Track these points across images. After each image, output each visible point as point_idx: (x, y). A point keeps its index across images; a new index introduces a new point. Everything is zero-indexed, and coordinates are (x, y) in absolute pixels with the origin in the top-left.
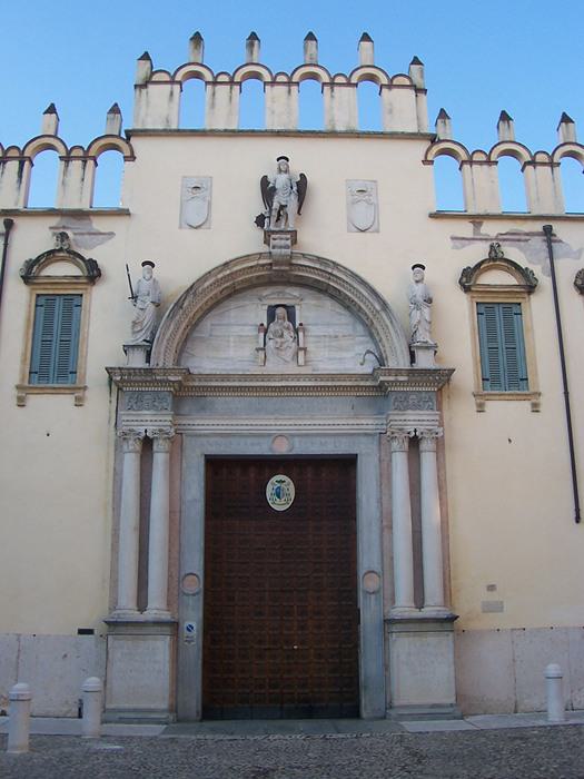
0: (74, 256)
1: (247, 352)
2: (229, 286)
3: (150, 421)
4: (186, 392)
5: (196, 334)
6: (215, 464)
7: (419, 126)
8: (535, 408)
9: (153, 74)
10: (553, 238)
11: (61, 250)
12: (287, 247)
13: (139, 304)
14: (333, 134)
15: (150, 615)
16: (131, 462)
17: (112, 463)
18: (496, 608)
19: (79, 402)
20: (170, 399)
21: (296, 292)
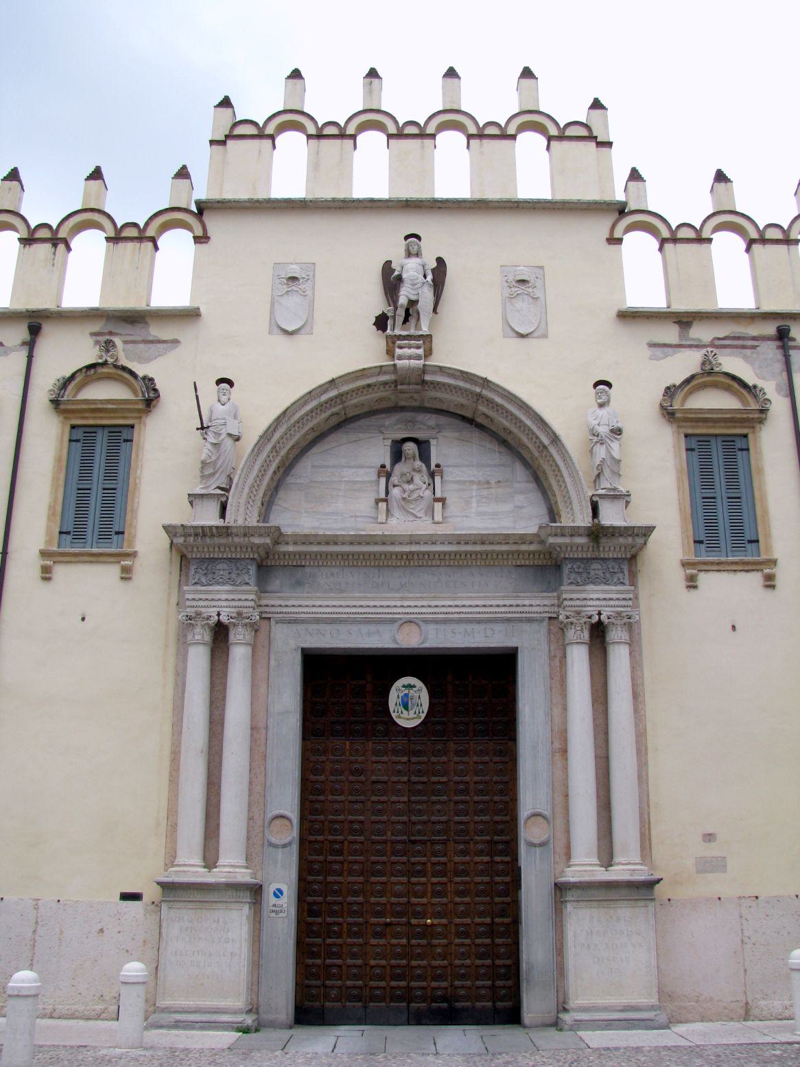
1: (364, 504)
2: (333, 417)
3: (224, 599)
5: (290, 480)
12: (418, 357)
16: (199, 658)
18: (715, 865)
19: (127, 574)
20: (253, 569)
21: (431, 420)
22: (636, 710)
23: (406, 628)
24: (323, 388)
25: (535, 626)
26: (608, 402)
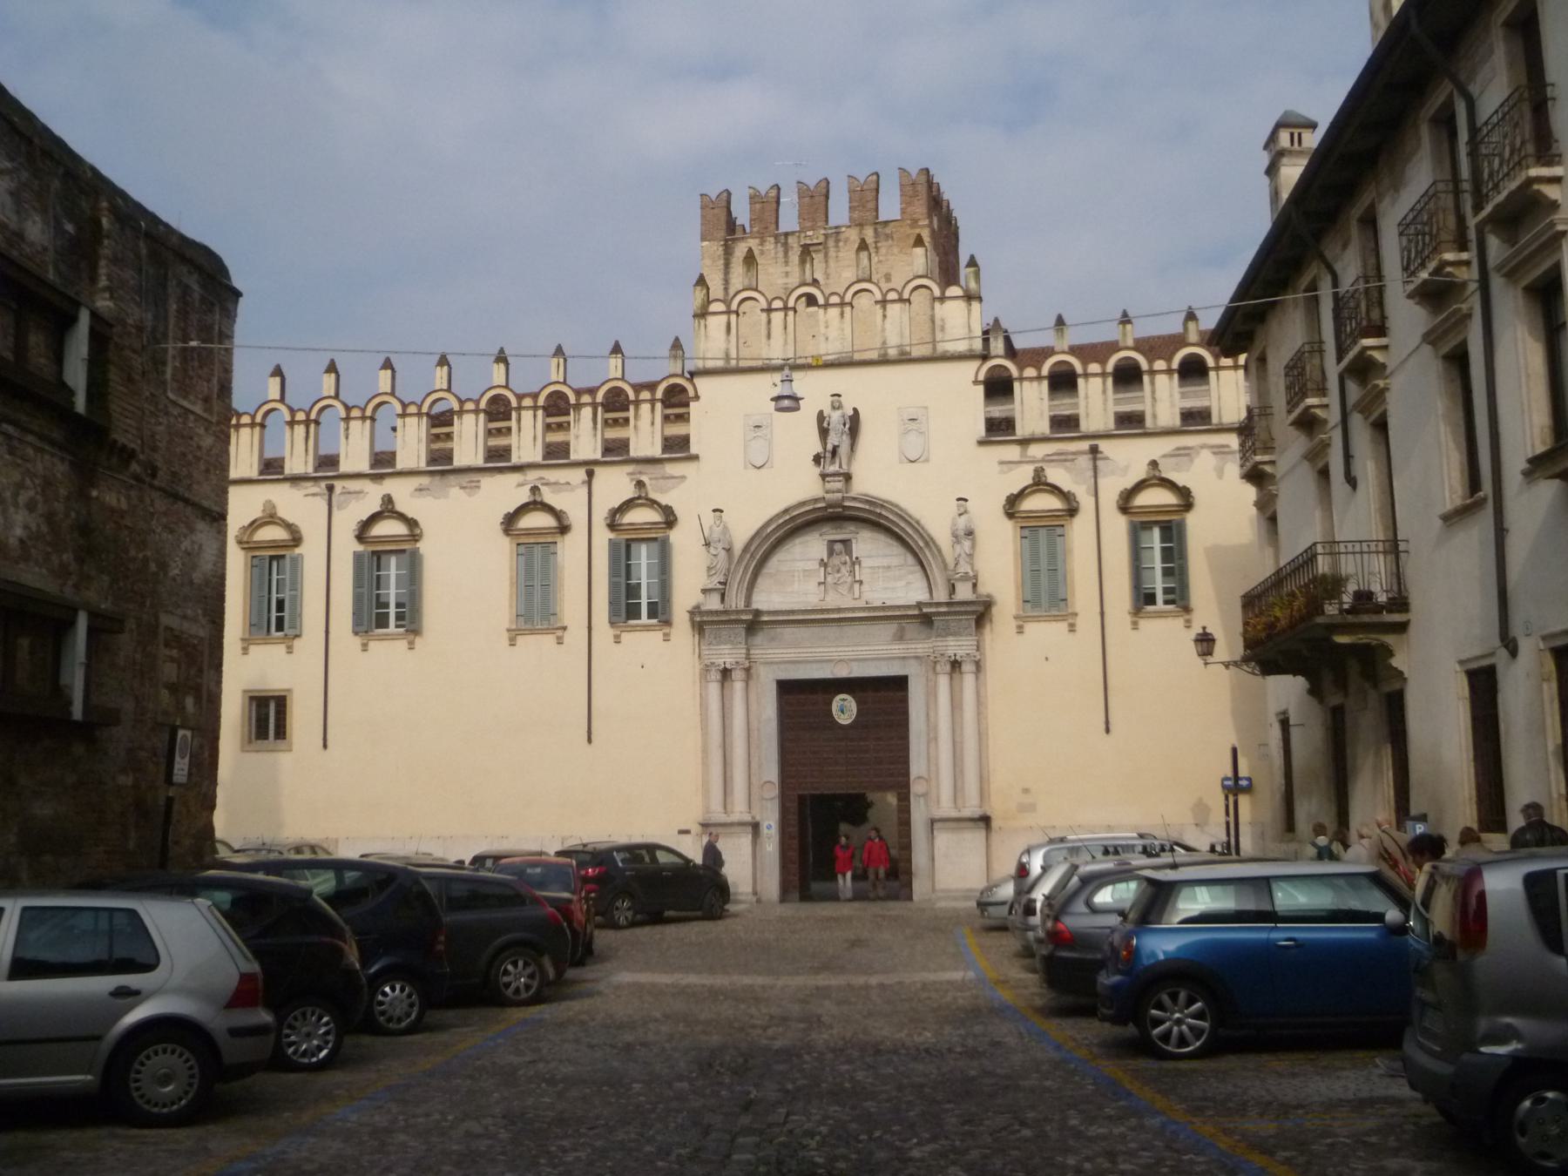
0: (653, 503)
1: (812, 586)
2: (796, 524)
3: (727, 653)
8: (1072, 628)
11: (639, 498)
13: (712, 550)
16: (714, 689)
18: (1031, 808)
21: (851, 527)
24: (778, 516)
26: (1279, 126)
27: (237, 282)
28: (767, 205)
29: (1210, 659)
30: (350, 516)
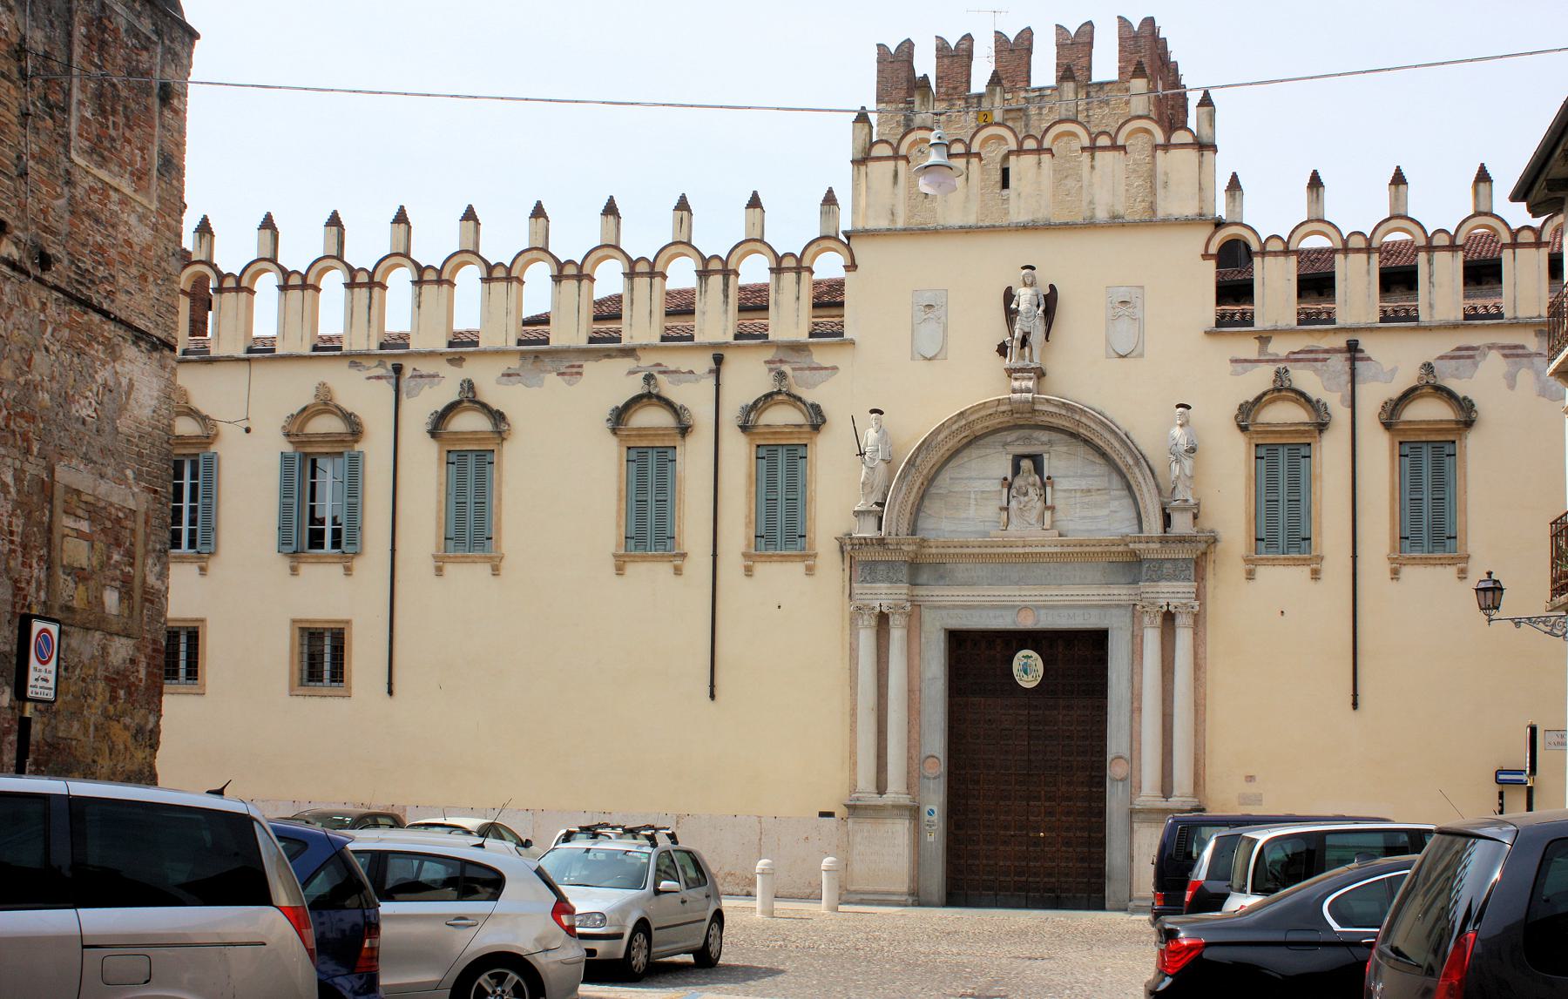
1: (991, 510)
2: (968, 435)
3: (884, 594)
4: (919, 567)
5: (933, 490)
6: (957, 639)
7: (1201, 200)
8: (1316, 575)
9: (872, 144)
10: (1359, 355)
11: (779, 392)
12: (1028, 391)
14: (1090, 225)
15: (889, 798)
16: (867, 639)
17: (847, 638)
19: (810, 571)
20: (905, 569)
21: (1044, 436)
22: (1196, 679)
23: (1023, 614)
25: (1122, 611)
27: (191, 18)
28: (956, 57)
29: (1495, 614)
30: (422, 404)
